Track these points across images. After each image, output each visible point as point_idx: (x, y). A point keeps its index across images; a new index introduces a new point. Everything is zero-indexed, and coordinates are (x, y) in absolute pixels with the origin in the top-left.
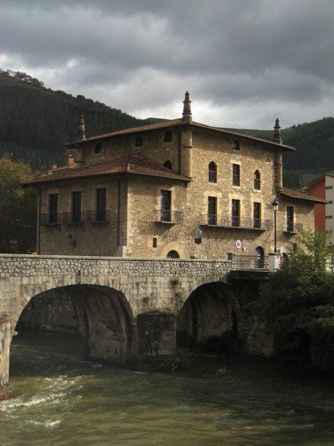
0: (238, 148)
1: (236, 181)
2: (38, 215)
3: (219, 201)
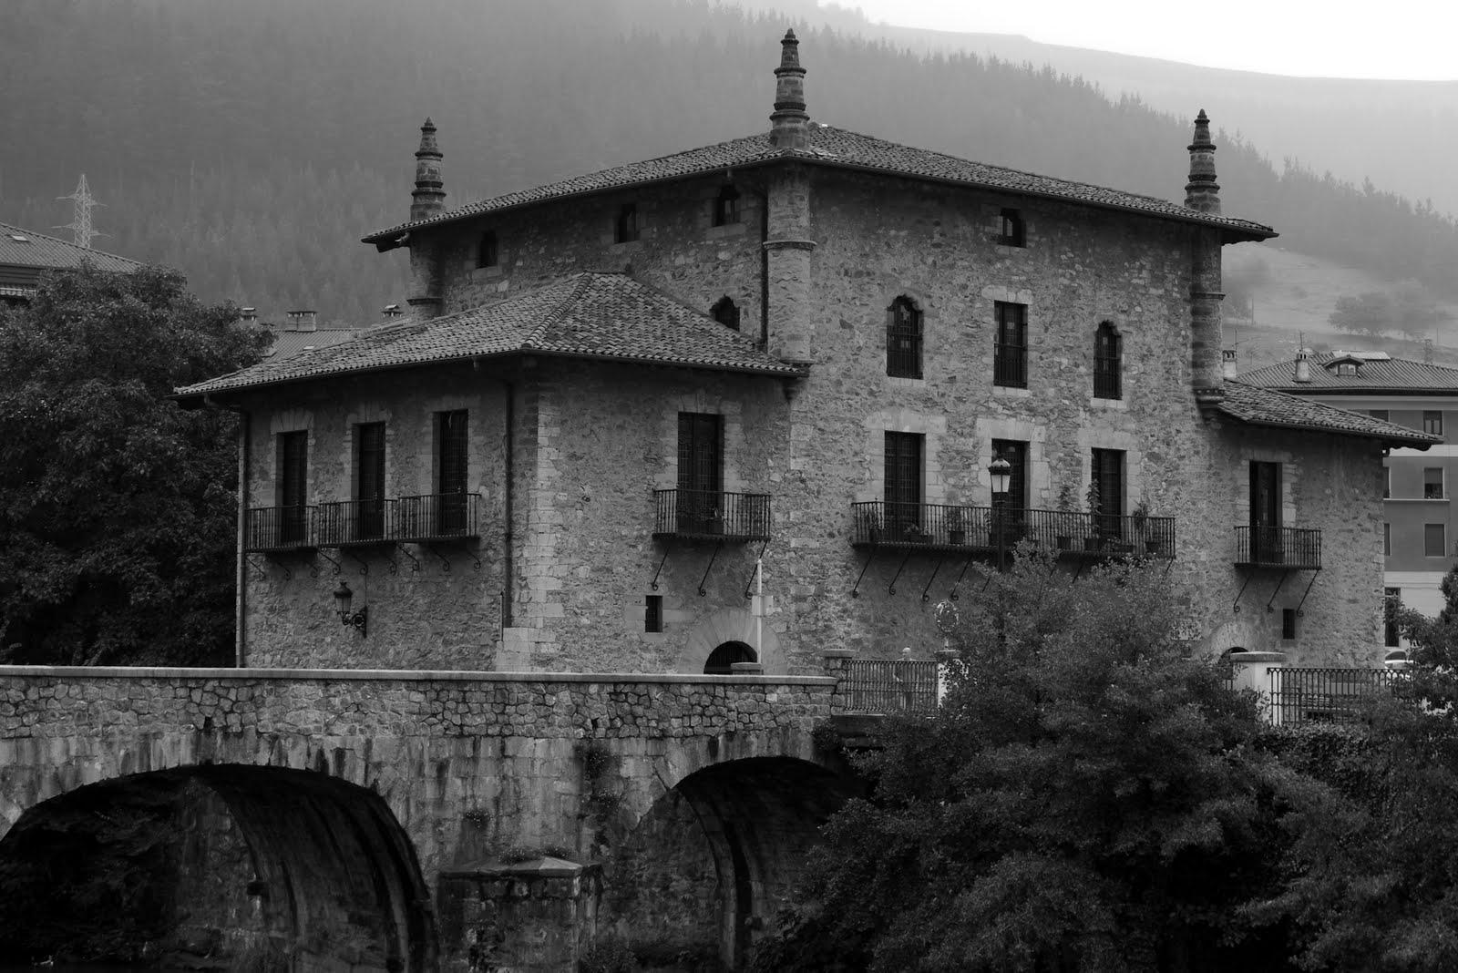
0: (1018, 240)
1: (1011, 368)
2: (240, 511)
3: (931, 449)
